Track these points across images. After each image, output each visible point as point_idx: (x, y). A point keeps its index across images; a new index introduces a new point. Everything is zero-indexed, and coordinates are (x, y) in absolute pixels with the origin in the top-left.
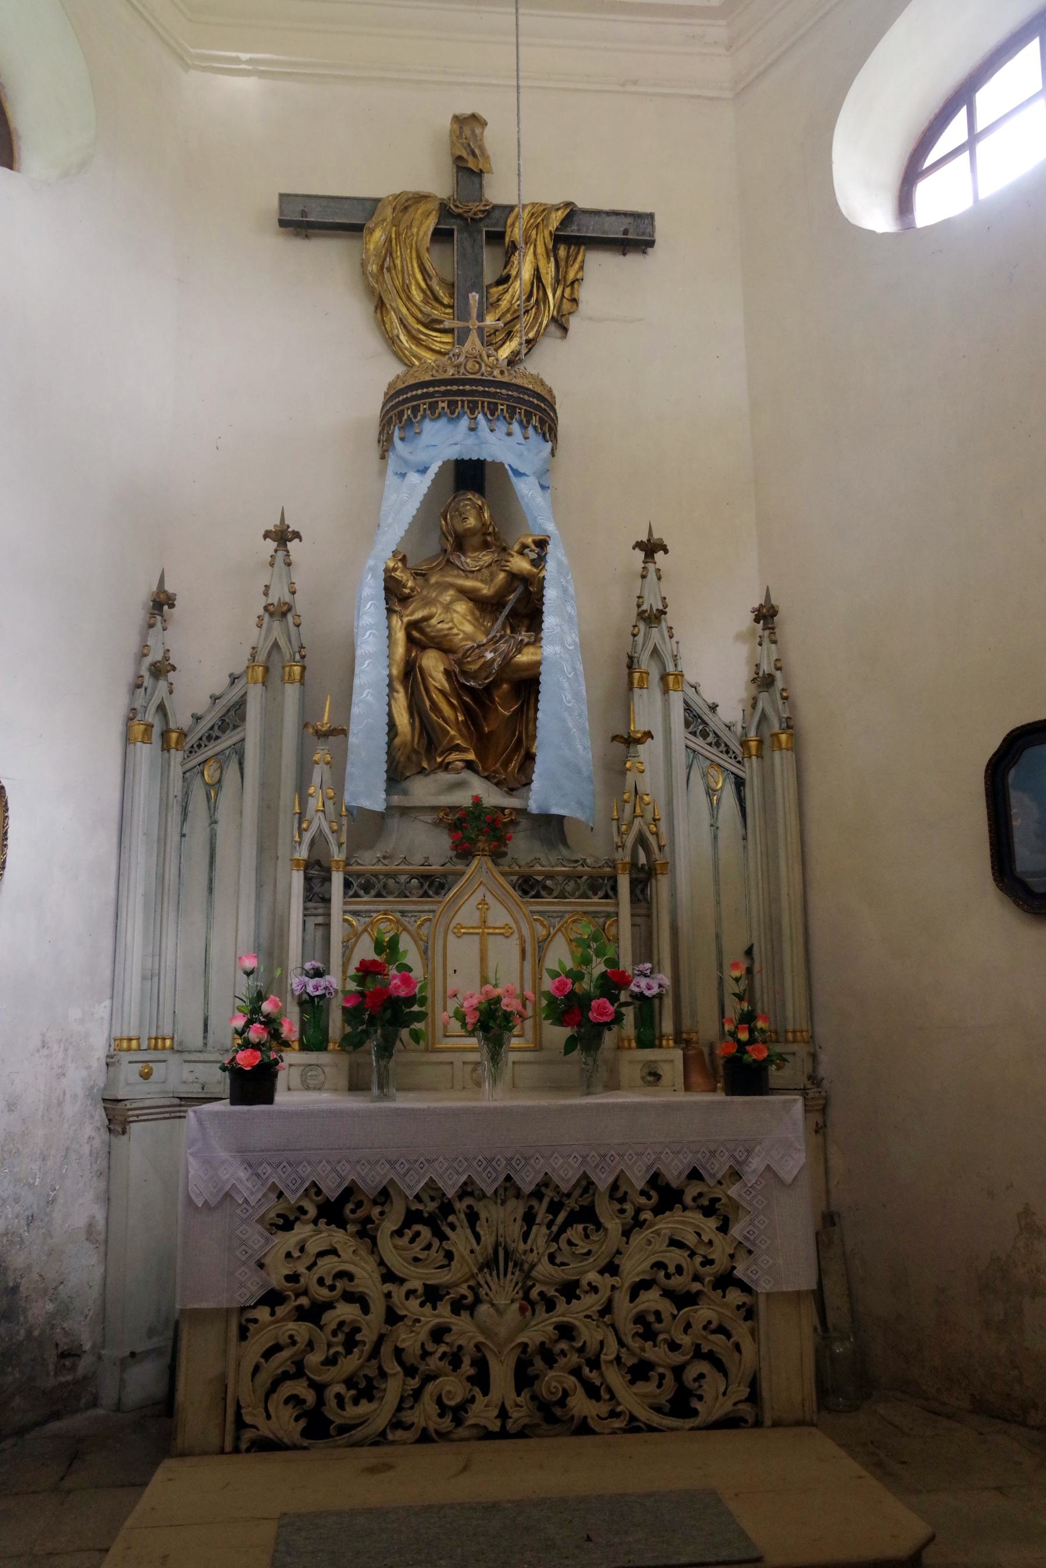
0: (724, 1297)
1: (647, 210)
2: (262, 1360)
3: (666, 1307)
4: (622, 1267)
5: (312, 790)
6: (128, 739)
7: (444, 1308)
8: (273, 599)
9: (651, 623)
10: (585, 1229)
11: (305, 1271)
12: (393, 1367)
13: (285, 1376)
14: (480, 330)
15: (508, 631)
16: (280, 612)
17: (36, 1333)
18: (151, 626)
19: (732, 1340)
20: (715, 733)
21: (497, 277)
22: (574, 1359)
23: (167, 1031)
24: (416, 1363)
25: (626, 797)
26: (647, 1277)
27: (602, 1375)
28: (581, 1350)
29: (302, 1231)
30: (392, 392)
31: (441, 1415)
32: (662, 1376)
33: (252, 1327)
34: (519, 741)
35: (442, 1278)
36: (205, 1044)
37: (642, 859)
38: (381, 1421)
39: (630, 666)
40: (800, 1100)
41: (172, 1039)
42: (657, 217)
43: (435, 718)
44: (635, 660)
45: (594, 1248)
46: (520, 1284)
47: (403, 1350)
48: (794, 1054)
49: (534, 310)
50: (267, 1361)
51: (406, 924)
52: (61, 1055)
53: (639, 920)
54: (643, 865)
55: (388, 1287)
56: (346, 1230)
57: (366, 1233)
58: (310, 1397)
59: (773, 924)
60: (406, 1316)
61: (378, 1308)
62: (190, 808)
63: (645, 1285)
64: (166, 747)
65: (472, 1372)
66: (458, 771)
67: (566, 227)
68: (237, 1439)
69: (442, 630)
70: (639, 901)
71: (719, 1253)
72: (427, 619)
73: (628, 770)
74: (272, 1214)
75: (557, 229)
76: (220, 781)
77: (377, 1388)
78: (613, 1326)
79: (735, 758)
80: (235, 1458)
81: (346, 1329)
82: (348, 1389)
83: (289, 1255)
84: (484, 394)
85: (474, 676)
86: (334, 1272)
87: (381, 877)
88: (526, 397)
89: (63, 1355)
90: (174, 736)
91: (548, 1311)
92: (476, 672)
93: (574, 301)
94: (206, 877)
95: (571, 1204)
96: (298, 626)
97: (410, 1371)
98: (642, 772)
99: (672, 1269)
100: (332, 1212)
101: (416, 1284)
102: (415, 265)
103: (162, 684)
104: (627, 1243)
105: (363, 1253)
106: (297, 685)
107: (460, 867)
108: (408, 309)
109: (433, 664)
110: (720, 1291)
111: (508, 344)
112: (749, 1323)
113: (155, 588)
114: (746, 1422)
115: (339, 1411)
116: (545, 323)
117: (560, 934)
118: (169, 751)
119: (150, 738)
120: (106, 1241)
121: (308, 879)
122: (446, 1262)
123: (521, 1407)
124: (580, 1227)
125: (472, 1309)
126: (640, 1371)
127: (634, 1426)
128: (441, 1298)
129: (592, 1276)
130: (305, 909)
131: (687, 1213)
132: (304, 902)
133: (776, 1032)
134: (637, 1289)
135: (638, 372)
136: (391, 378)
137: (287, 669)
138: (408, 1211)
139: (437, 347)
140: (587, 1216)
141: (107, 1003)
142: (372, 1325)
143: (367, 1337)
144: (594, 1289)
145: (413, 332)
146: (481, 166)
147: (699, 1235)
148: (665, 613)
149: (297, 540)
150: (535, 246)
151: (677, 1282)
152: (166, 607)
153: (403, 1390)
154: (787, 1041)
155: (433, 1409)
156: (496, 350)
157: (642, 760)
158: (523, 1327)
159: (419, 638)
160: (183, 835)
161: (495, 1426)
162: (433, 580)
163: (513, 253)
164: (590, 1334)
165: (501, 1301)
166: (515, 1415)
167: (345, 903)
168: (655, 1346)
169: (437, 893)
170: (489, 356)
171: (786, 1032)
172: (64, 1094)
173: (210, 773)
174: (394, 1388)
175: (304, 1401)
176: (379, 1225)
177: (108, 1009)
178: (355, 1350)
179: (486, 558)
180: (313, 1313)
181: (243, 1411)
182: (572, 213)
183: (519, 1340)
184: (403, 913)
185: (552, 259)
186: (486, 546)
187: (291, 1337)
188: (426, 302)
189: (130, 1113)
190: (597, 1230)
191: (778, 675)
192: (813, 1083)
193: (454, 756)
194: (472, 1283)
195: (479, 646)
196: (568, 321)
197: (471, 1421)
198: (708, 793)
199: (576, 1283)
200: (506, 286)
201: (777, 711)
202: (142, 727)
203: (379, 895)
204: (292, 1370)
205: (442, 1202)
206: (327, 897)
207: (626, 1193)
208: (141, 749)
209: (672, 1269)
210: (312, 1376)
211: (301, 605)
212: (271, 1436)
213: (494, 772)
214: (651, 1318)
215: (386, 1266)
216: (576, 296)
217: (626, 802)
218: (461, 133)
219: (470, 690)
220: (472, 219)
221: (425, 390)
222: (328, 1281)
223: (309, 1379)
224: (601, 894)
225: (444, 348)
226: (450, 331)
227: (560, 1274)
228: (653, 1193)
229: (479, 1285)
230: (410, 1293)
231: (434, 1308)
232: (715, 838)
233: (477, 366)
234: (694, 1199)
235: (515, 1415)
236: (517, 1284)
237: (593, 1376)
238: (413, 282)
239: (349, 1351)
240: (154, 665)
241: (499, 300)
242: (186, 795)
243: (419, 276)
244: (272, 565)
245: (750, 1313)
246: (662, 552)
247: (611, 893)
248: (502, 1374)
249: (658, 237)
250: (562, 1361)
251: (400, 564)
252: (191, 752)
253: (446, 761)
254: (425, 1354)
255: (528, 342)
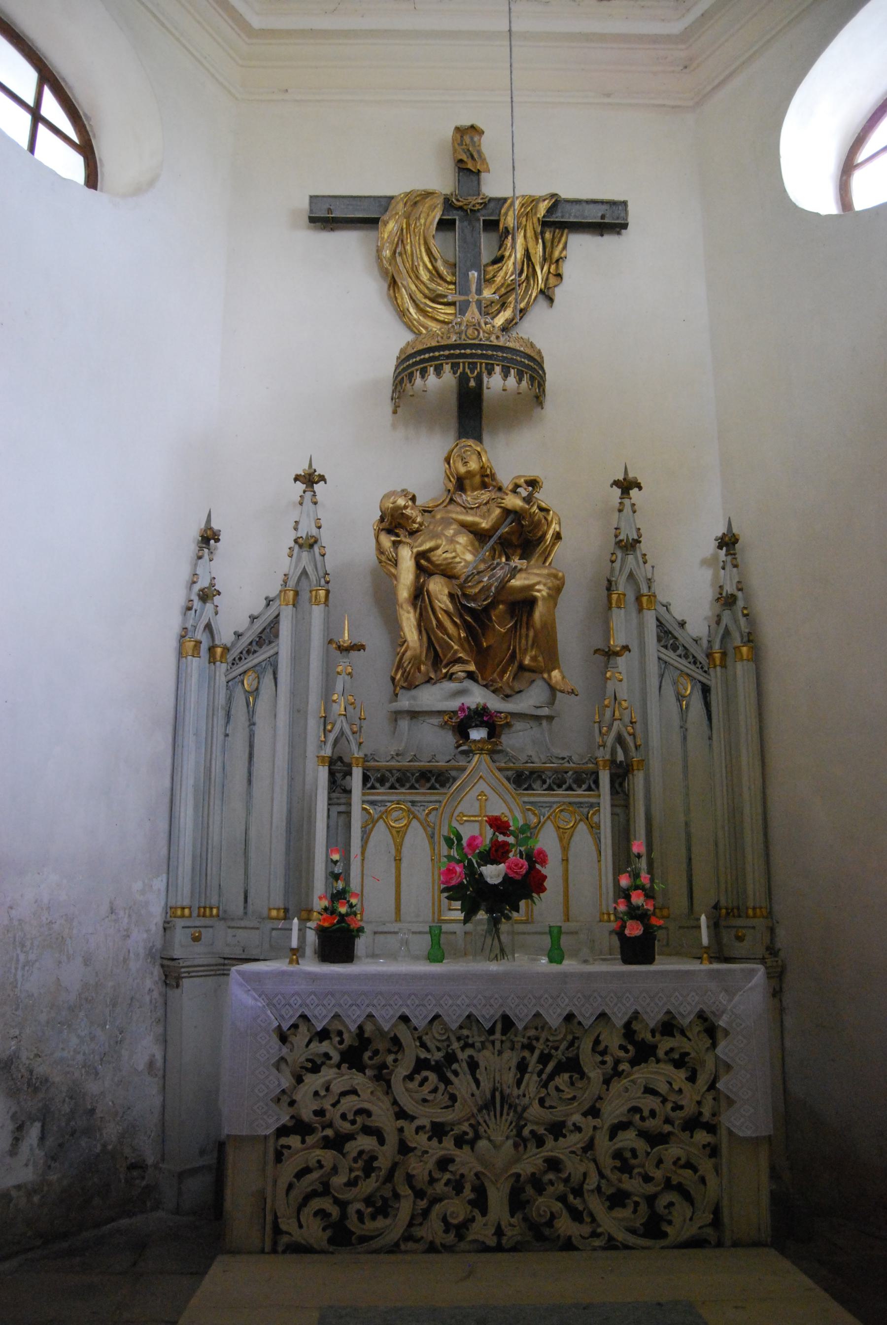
0: (692, 1137)
1: (621, 198)
2: (295, 1180)
3: (641, 1145)
4: (603, 1111)
5: (335, 697)
6: (181, 654)
7: (449, 1142)
8: (302, 533)
9: (627, 550)
10: (571, 1077)
11: (330, 1107)
12: (405, 1190)
13: (314, 1194)
14: (479, 303)
15: (504, 560)
16: (308, 544)
17: (110, 1147)
18: (200, 558)
19: (698, 1174)
20: (683, 646)
21: (492, 258)
22: (561, 1187)
23: (214, 901)
24: (424, 1187)
25: (606, 702)
26: (624, 1119)
27: (584, 1202)
28: (567, 1181)
29: (327, 1073)
30: (403, 357)
31: (446, 1231)
32: (637, 1204)
33: (285, 1151)
34: (513, 656)
35: (448, 1117)
36: (246, 913)
37: (620, 757)
38: (396, 1234)
39: (609, 589)
40: (761, 969)
41: (218, 908)
42: (629, 204)
43: (441, 635)
44: (613, 583)
45: (578, 1094)
46: (514, 1124)
47: (414, 1176)
48: (754, 928)
49: (524, 284)
50: (298, 1180)
51: (416, 812)
52: (126, 920)
53: (618, 810)
54: (621, 762)
55: (401, 1123)
56: (365, 1074)
57: (382, 1077)
58: (335, 1211)
59: (735, 812)
60: (415, 1148)
61: (392, 1140)
62: (233, 712)
63: (623, 1126)
64: (212, 660)
65: (472, 1196)
66: (461, 681)
67: (552, 214)
68: (275, 1243)
69: (446, 559)
70: (618, 793)
71: (688, 1100)
72: (432, 550)
73: (608, 679)
74: (303, 1059)
75: (544, 217)
76: (257, 689)
77: (392, 1207)
78: (595, 1161)
79: (702, 668)
80: (273, 1257)
81: (365, 1157)
82: (367, 1206)
83: (316, 1094)
84: (482, 356)
85: (473, 598)
86: (355, 1109)
87: (394, 772)
88: (518, 358)
89: (132, 1167)
90: (219, 651)
91: (538, 1147)
92: (475, 594)
93: (559, 276)
94: (246, 770)
95: (559, 1055)
96: (323, 555)
97: (419, 1194)
98: (621, 681)
99: (646, 1113)
100: (352, 1058)
101: (425, 1122)
102: (423, 250)
103: (209, 606)
104: (608, 1090)
105: (379, 1094)
106: (322, 606)
107: (462, 763)
108: (416, 286)
109: (438, 587)
110: (687, 1132)
111: (502, 313)
112: (713, 1160)
113: (203, 526)
114: (710, 1243)
115: (359, 1224)
116: (534, 294)
117: (549, 822)
118: (214, 663)
119: (199, 653)
120: (164, 1077)
121: (332, 773)
122: (449, 1103)
123: (515, 1226)
124: (566, 1076)
125: (472, 1143)
126: (617, 1199)
127: (612, 1245)
128: (446, 1134)
129: (577, 1118)
130: (329, 799)
131: (662, 1065)
132: (329, 793)
133: (738, 909)
134: (615, 1130)
135: (619, 333)
136: (402, 344)
137: (314, 593)
138: (418, 1059)
139: (441, 317)
140: (572, 1066)
141: (165, 876)
142: (386, 1155)
143: (383, 1163)
144: (578, 1129)
145: (422, 306)
146: (478, 167)
147: (670, 1084)
148: (640, 542)
149: (322, 483)
150: (525, 231)
151: (651, 1124)
152: (212, 542)
153: (414, 1209)
154: (747, 917)
155: (439, 1226)
156: (493, 319)
157: (620, 670)
158: (517, 1160)
159: (425, 566)
160: (227, 735)
161: (492, 1242)
162: (439, 516)
163: (506, 237)
164: (574, 1167)
165: (499, 1138)
166: (509, 1233)
167: (364, 794)
168: (631, 1178)
169: (443, 785)
170: (486, 323)
171: (747, 908)
172: (129, 952)
173: (249, 682)
174: (405, 1208)
175: (330, 1215)
176: (393, 1071)
177: (165, 881)
178: (373, 1175)
179: (485, 496)
180: (337, 1143)
181: (280, 1220)
182: (556, 203)
183: (514, 1171)
184: (413, 803)
185: (540, 241)
186: (484, 486)
187: (319, 1162)
188: (431, 280)
189: (183, 970)
190: (582, 1078)
191: (739, 594)
192: (771, 954)
193: (456, 668)
194: (472, 1121)
195: (479, 573)
196: (554, 292)
197: (470, 1238)
198: (678, 700)
199: (563, 1124)
200: (500, 265)
201: (739, 627)
202: (192, 643)
203: (392, 787)
204: (320, 1189)
205: (447, 1052)
206: (348, 789)
207: (607, 1047)
208: (192, 661)
209: (646, 1113)
210: (336, 1194)
211: (325, 538)
212: (303, 1241)
213: (492, 681)
214: (628, 1155)
215: (399, 1105)
216: (560, 272)
217: (607, 706)
218: (462, 141)
219: (471, 611)
220: (471, 210)
221: (431, 354)
222: (350, 1117)
223: (334, 1197)
224: (584, 787)
225: (447, 318)
226: (453, 304)
227: (547, 1116)
228: (630, 1047)
229: (479, 1124)
230: (419, 1129)
231: (440, 1142)
232: (685, 738)
233: (476, 333)
234: (666, 1053)
235: (509, 1233)
236: (511, 1123)
237: (577, 1202)
238: (421, 264)
239: (368, 1176)
240: (202, 590)
241: (494, 276)
242: (229, 700)
243: (426, 259)
244: (301, 504)
245: (713, 1151)
246: (636, 490)
247: (593, 786)
248: (498, 1197)
249: (631, 220)
250: (550, 1189)
251: (410, 503)
252: (233, 664)
253: (451, 671)
254: (432, 1181)
255: (521, 311)
